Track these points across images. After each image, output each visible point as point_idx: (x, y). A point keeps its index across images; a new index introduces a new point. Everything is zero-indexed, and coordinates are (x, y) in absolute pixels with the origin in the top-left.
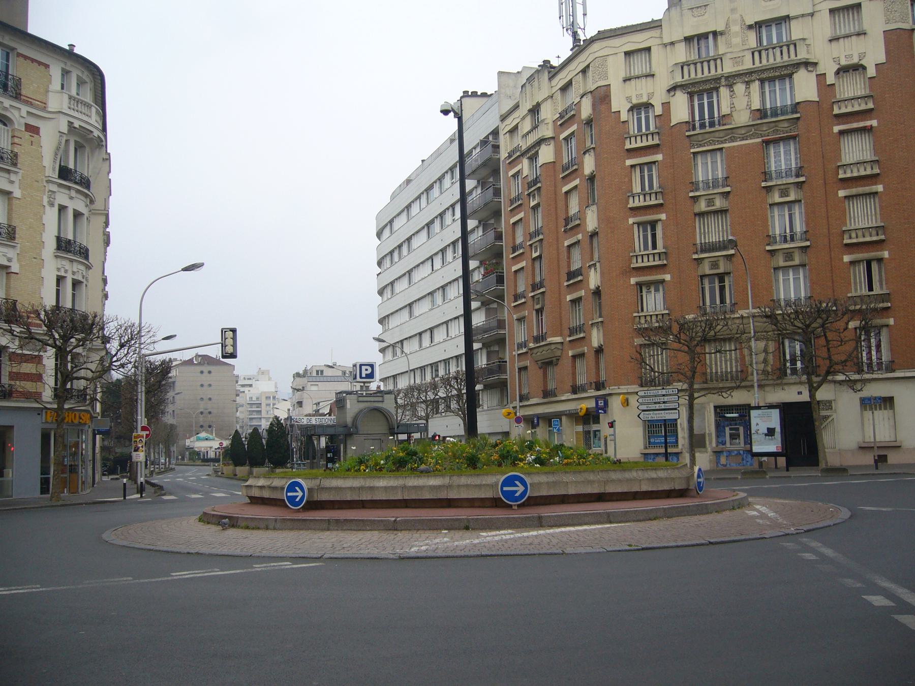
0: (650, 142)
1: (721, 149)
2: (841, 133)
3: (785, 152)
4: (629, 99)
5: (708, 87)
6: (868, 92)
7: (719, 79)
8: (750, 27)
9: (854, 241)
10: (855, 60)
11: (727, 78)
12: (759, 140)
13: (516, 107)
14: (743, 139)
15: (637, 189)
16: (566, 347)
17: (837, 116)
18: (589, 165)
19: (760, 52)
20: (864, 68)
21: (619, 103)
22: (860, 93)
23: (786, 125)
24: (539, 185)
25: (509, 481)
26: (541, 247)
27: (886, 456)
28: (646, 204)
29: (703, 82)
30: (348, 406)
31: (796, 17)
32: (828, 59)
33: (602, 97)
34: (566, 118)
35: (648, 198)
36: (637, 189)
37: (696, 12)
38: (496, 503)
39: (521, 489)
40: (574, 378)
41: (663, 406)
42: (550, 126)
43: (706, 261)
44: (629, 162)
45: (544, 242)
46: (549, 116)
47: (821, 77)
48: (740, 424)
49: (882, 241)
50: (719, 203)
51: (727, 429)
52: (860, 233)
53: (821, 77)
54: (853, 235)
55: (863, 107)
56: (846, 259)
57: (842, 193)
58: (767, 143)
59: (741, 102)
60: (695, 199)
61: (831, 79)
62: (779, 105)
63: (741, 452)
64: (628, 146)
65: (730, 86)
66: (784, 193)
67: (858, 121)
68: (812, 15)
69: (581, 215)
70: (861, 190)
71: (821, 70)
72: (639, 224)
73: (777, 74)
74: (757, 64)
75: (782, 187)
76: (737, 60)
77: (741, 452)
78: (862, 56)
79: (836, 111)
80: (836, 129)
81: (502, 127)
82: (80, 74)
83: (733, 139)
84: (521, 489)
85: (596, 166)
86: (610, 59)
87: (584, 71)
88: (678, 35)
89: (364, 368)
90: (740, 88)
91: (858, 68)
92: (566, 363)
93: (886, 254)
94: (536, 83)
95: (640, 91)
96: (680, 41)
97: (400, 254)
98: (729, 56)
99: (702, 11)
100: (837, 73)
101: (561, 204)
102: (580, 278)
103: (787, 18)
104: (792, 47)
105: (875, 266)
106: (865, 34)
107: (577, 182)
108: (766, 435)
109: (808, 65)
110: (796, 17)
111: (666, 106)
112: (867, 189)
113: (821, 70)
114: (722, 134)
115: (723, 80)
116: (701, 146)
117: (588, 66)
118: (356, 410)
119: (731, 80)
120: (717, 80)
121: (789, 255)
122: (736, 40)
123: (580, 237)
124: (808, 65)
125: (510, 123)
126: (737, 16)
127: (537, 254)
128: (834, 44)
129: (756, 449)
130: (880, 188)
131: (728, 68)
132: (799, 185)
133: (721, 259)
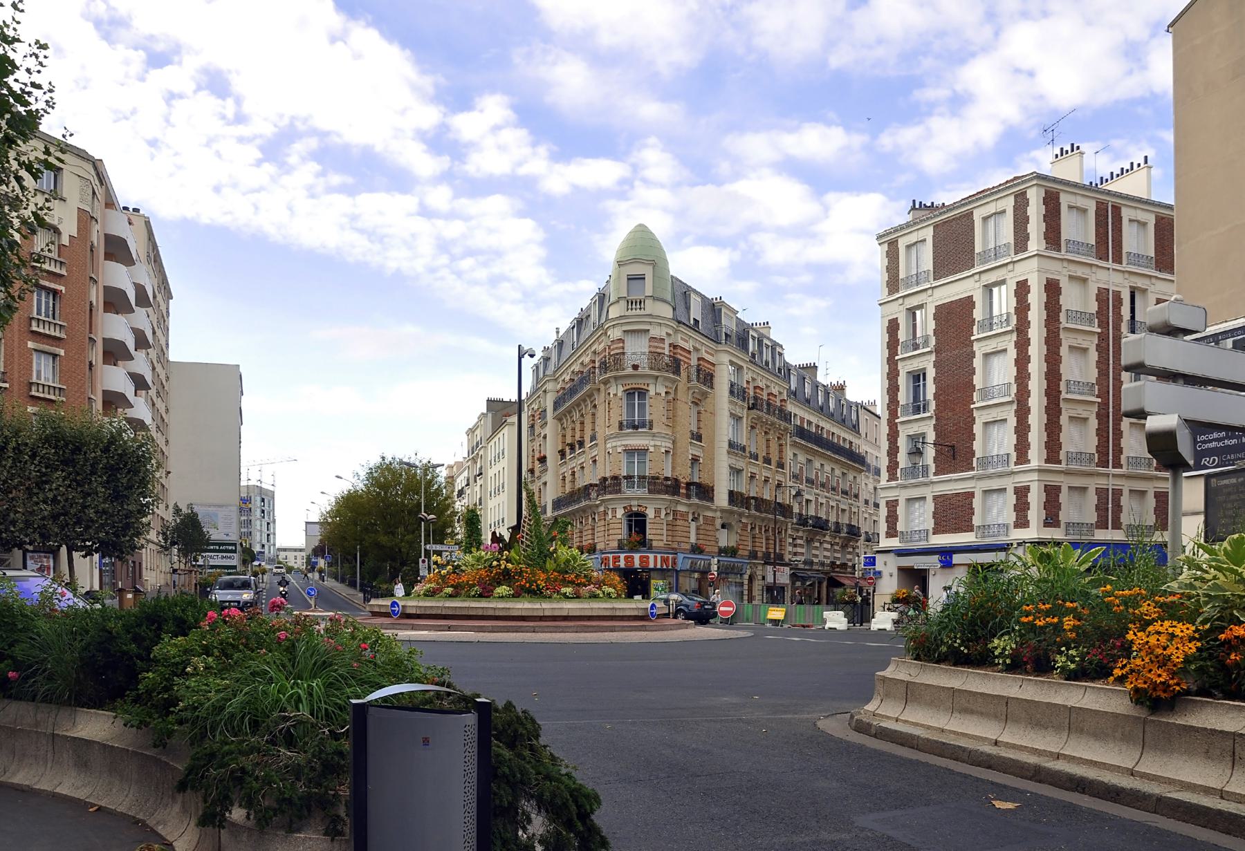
9: (42, 395)
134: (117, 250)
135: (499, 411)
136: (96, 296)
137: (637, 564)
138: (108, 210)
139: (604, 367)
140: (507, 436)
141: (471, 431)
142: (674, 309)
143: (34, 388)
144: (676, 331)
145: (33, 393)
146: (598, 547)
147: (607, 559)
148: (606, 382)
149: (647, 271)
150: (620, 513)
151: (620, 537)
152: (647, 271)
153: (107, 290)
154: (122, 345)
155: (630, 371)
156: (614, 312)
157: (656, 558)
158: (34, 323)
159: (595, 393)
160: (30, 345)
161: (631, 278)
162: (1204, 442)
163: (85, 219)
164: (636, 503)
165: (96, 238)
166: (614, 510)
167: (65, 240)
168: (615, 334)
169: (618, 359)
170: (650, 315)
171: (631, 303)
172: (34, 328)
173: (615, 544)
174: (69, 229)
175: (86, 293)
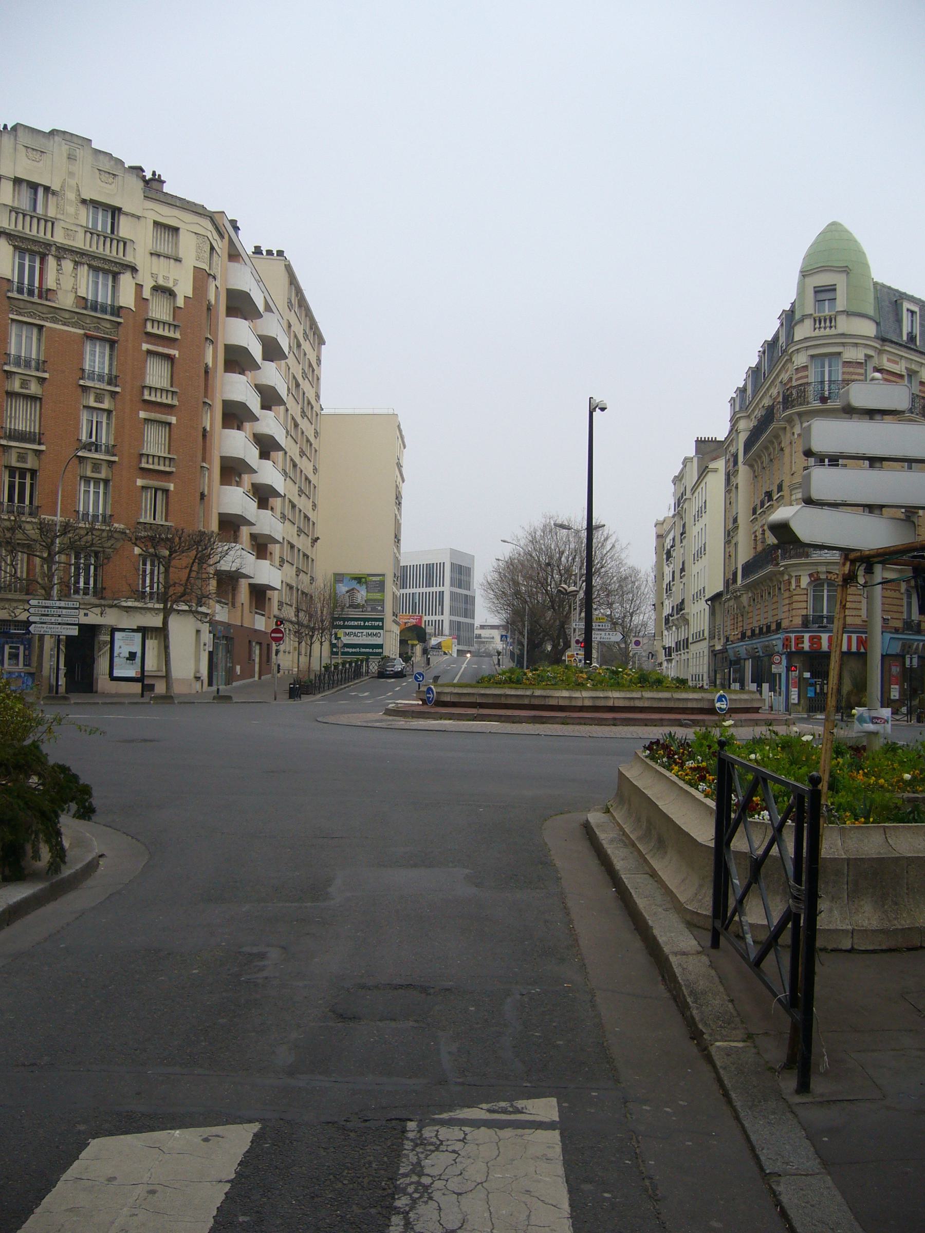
1: (40, 327)
2: (149, 352)
3: (91, 351)
5: (36, 248)
7: (50, 245)
9: (151, 467)
10: (170, 285)
11: (58, 248)
12: (82, 332)
14: (64, 324)
17: (148, 334)
19: (112, 240)
23: (108, 326)
27: (153, 685)
29: (116, 263)
31: (127, 214)
37: (31, 154)
41: (60, 620)
43: (89, 461)
48: (22, 643)
49: (170, 473)
50: (34, 388)
51: (7, 647)
54: (151, 460)
56: (140, 482)
58: (88, 337)
61: (147, 293)
62: (99, 300)
63: (23, 674)
65: (59, 259)
66: (99, 399)
67: (164, 346)
73: (106, 267)
75: (98, 391)
77: (23, 674)
79: (149, 329)
82: (908, 366)
83: (54, 320)
90: (68, 265)
93: (172, 487)
96: (8, 178)
98: (62, 224)
99: (37, 156)
105: (159, 494)
106: (151, 254)
108: (127, 659)
112: (164, 418)
114: (45, 310)
115: (53, 249)
119: (63, 252)
120: (48, 245)
121: (96, 467)
126: (73, 182)
128: (155, 258)
129: (117, 673)
133: (30, 452)
134: (240, 305)
135: (707, 449)
136: (212, 357)
137: (806, 646)
138: (232, 264)
139: (787, 401)
140: (715, 483)
141: (678, 480)
142: (878, 324)
143: (144, 460)
144: (880, 352)
145: (144, 465)
146: (783, 625)
147: (788, 639)
148: (790, 420)
149: (839, 280)
150: (805, 581)
151: (804, 612)
152: (839, 280)
153: (229, 349)
154: (243, 406)
155: (817, 405)
156: (801, 332)
157: (849, 639)
158: (146, 392)
159: (781, 433)
160: (142, 415)
161: (818, 291)
162: (22, 572)
163: (202, 277)
164: (823, 569)
165: (214, 294)
166: (798, 578)
167: (180, 302)
168: (801, 359)
169: (802, 389)
170: (843, 335)
171: (818, 321)
172: (147, 397)
173: (798, 621)
174: (185, 290)
175: (202, 354)
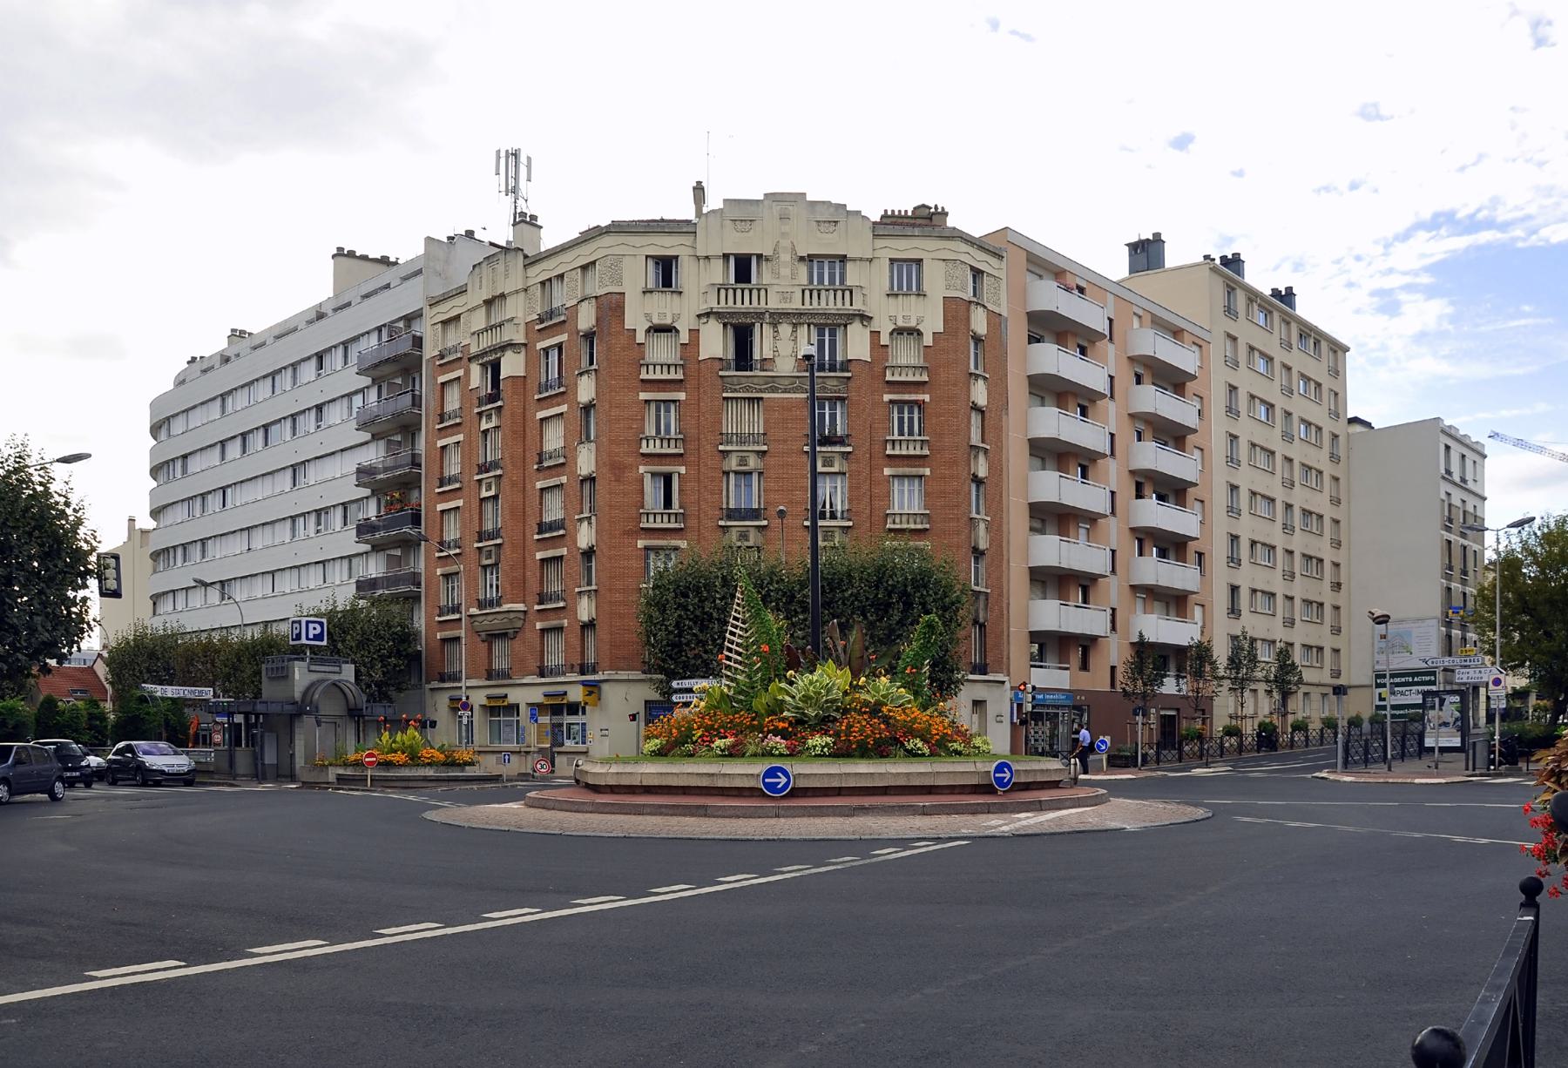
0: (672, 376)
4: (648, 316)
6: (922, 363)
8: (802, 259)
11: (772, 315)
13: (462, 291)
14: (785, 391)
15: (650, 430)
16: (530, 617)
18: (586, 390)
20: (920, 333)
21: (636, 318)
22: (913, 362)
24: (499, 403)
25: (771, 772)
26: (498, 486)
28: (663, 451)
30: (297, 676)
31: (854, 260)
32: (887, 313)
33: (611, 307)
34: (549, 321)
35: (665, 444)
36: (650, 430)
38: (987, 789)
39: (784, 780)
40: (490, 663)
42: (522, 328)
44: (643, 396)
45: (504, 480)
46: (520, 315)
47: (875, 334)
52: (904, 518)
53: (875, 334)
55: (917, 378)
57: (887, 471)
59: (785, 347)
60: (725, 453)
61: (885, 340)
64: (644, 376)
65: (775, 325)
68: (870, 260)
69: (568, 453)
70: (907, 471)
71: (875, 326)
72: (653, 474)
74: (807, 306)
76: (785, 296)
78: (676, 317)
79: (889, 378)
80: (887, 397)
81: (427, 312)
83: (774, 390)
84: (784, 780)
85: (597, 393)
86: (626, 260)
87: (584, 268)
88: (716, 250)
89: (311, 626)
90: (785, 329)
91: (914, 332)
92: (531, 637)
94: (500, 267)
95: (663, 308)
97: (184, 470)
100: (648, 331)
101: (532, 433)
102: (562, 532)
103: (843, 259)
104: (847, 294)
107: (564, 408)
109: (864, 318)
110: (854, 260)
111: (695, 333)
112: (914, 471)
113: (875, 326)
116: (735, 391)
117: (594, 263)
118: (306, 683)
119: (777, 318)
122: (786, 271)
123: (564, 479)
124: (864, 318)
125: (447, 310)
126: (785, 243)
127: (492, 493)
130: (927, 471)
131: (774, 303)
132: (845, 455)
